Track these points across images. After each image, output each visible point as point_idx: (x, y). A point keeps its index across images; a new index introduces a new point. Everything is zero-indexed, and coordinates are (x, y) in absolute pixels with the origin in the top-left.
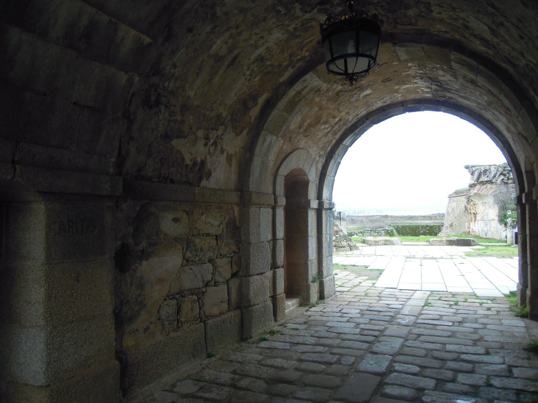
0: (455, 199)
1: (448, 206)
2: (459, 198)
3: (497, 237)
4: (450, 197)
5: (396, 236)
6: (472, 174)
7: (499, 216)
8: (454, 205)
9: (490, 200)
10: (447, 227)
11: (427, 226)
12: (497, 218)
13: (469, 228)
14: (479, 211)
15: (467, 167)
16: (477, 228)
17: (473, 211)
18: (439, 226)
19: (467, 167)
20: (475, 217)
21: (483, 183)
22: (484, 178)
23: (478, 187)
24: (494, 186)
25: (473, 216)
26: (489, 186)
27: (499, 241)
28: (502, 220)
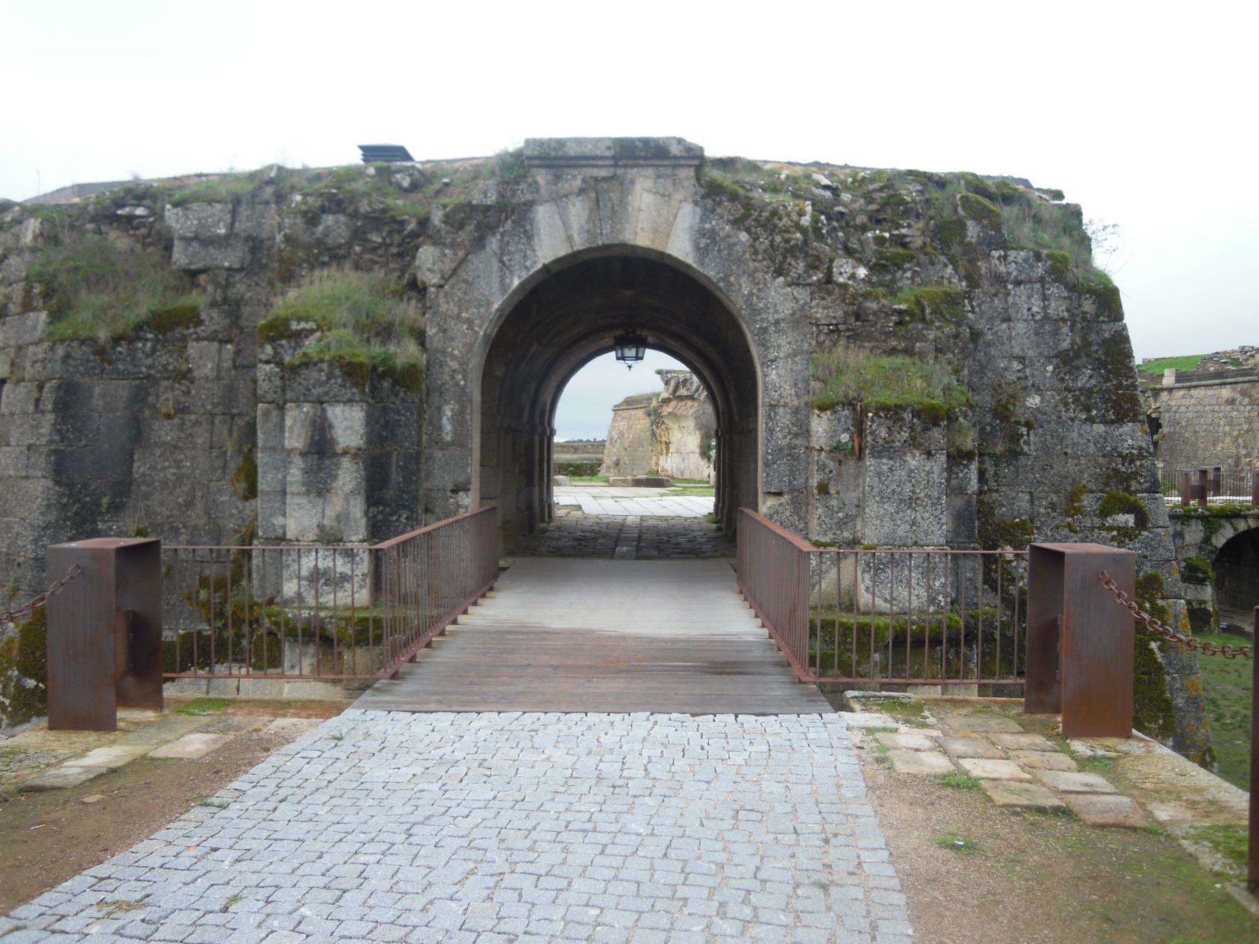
0: (626, 414)
1: (612, 428)
2: (633, 412)
3: (697, 477)
4: (616, 409)
5: (481, 505)
6: (667, 383)
7: (701, 447)
8: (622, 425)
9: (690, 423)
10: (608, 467)
11: (571, 465)
12: (698, 450)
13: (657, 464)
14: (673, 439)
15: (659, 372)
16: (669, 464)
17: (664, 439)
18: (592, 466)
19: (659, 372)
20: (668, 449)
21: (681, 398)
22: (683, 392)
23: (673, 403)
24: (696, 404)
25: (664, 446)
26: (689, 403)
27: (699, 482)
28: (704, 453)
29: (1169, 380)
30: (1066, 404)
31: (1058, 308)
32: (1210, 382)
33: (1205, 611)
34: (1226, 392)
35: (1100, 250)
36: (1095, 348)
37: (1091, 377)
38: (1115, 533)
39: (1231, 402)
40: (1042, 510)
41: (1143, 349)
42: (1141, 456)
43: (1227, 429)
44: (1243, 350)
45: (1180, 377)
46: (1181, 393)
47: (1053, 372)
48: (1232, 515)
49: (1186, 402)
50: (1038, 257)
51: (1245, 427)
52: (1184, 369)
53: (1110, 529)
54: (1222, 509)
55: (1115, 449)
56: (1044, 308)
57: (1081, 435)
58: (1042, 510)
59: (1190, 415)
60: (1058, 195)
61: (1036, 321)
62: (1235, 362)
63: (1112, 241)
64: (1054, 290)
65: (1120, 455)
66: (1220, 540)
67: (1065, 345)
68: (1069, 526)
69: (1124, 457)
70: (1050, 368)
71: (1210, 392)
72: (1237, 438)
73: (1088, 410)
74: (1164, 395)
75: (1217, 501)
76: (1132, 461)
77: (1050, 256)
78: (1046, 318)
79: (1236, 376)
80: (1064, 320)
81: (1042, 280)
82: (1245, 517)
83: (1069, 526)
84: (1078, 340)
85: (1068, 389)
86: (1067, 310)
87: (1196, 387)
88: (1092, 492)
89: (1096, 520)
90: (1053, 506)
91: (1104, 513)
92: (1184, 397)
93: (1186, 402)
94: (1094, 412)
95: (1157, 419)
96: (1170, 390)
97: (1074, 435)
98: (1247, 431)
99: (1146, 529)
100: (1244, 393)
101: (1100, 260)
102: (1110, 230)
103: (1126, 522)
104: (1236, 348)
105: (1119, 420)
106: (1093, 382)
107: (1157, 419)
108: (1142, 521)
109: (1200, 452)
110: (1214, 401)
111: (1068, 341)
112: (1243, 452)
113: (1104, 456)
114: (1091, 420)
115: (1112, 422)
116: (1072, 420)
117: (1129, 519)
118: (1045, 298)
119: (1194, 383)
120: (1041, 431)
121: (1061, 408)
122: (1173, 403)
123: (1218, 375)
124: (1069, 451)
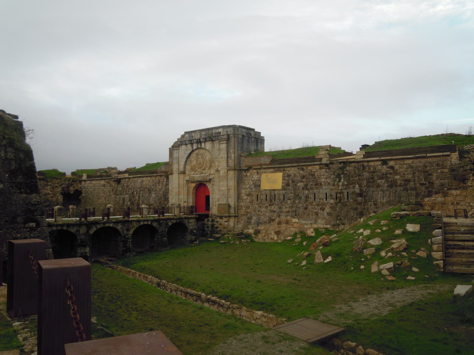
29: (85, 177)
30: (13, 188)
31: (10, 155)
32: (97, 179)
33: (87, 256)
34: (102, 182)
35: (28, 137)
36: (24, 169)
37: (22, 178)
38: (29, 229)
39: (104, 185)
40: (2, 223)
41: (38, 168)
42: (38, 204)
43: (103, 194)
44: (109, 168)
45: (88, 176)
46: (89, 182)
47: (8, 177)
48: (95, 223)
49: (91, 185)
50: (4, 138)
51: (108, 194)
52: (90, 174)
53: (27, 228)
54: (92, 221)
55: (29, 202)
56: (6, 155)
57: (17, 198)
58: (2, 223)
59: (91, 190)
60: (16, 117)
61: (2, 159)
62: (106, 172)
63: (31, 135)
64: (9, 149)
65: (31, 204)
66: (92, 232)
67: (13, 168)
68: (13, 228)
69: (32, 205)
70: (7, 175)
71: (98, 182)
72: (106, 197)
73: (20, 189)
74: (83, 183)
75: (92, 218)
76: (35, 206)
77: (8, 138)
78: (6, 159)
79: (105, 177)
80: (12, 159)
81: (5, 146)
82: (100, 224)
83: (13, 228)
84: (17, 166)
85: (13, 182)
86: (14, 156)
87: (93, 180)
88: (21, 216)
89: (22, 225)
90: (6, 221)
91: (25, 223)
92: (89, 183)
93: (91, 185)
94: (23, 190)
95: (81, 191)
96: (85, 181)
97: (15, 197)
98: (109, 195)
99: (39, 227)
100: (108, 183)
101: (28, 141)
102: (31, 131)
103: (33, 225)
104: (106, 167)
105: (31, 193)
106: (22, 180)
107: (81, 191)
108: (38, 225)
109: (94, 203)
110: (99, 185)
111: (14, 166)
112: (107, 202)
113: (26, 204)
114: (21, 193)
115: (29, 193)
116: (15, 192)
117: (34, 225)
118: (6, 152)
119: (93, 179)
120: (3, 196)
121: (11, 188)
122: (86, 185)
123: (100, 176)
124: (13, 203)
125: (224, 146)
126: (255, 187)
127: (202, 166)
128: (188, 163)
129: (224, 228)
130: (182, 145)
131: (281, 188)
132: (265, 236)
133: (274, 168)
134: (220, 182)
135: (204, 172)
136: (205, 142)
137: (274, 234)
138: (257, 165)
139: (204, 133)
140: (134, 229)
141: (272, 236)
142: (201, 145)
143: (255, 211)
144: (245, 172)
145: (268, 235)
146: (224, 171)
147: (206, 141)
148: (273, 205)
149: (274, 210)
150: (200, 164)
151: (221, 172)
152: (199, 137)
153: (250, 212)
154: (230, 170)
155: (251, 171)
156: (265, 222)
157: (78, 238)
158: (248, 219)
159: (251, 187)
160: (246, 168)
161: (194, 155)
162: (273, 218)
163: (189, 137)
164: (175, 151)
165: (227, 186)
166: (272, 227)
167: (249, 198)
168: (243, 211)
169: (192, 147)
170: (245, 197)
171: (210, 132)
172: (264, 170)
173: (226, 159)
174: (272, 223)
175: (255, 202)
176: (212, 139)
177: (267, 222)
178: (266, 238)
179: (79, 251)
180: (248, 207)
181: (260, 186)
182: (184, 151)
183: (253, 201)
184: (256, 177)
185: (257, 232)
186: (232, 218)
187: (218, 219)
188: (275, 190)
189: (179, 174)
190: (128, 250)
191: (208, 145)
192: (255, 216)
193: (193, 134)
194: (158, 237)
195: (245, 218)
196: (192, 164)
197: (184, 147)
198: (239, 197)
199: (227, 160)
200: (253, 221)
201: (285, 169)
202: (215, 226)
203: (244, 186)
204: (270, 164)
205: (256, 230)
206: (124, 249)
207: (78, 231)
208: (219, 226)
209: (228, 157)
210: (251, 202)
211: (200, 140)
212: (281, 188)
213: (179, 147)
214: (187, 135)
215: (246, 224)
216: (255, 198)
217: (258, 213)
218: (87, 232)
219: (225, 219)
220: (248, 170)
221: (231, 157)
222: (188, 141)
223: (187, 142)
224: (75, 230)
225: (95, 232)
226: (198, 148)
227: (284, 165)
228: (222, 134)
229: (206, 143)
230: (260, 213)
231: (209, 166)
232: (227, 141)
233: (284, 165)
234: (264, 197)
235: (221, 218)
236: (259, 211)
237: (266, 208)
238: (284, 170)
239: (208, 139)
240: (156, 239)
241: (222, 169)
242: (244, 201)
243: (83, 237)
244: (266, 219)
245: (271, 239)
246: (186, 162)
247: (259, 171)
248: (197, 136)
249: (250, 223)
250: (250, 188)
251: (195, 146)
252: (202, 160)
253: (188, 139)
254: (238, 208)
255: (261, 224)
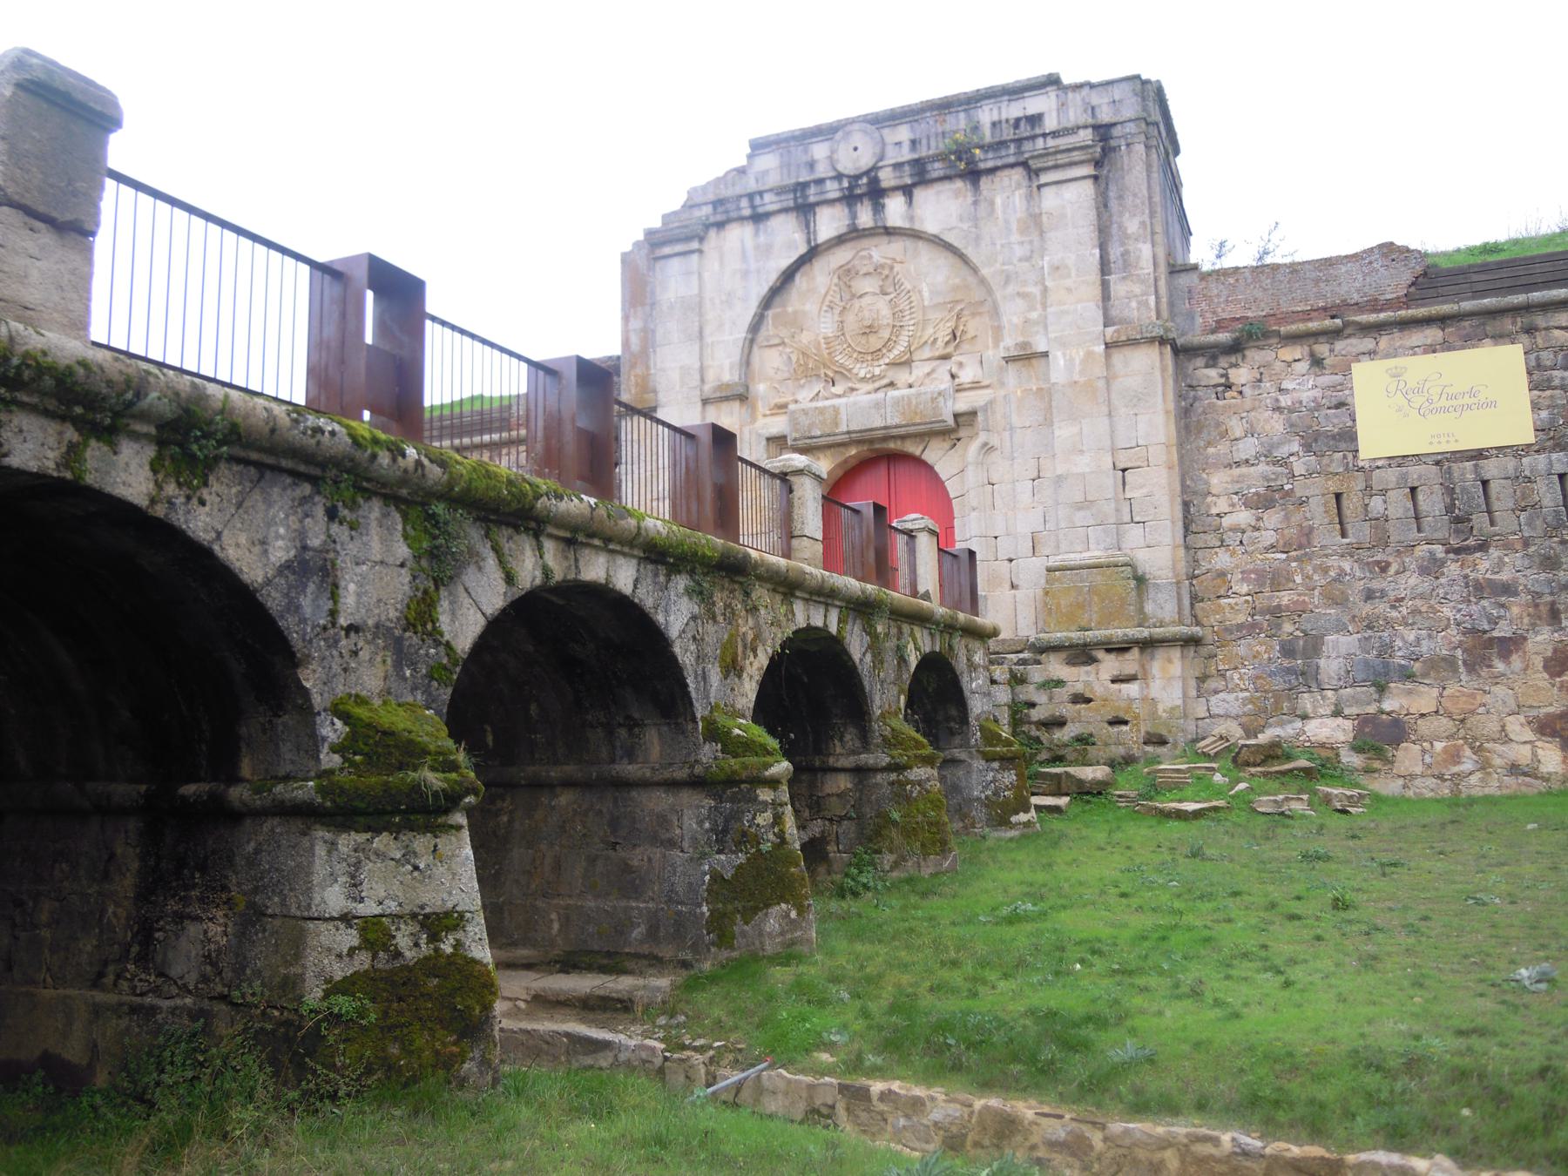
125: (1070, 199)
126: (1307, 448)
127: (888, 344)
128: (769, 330)
129: (1118, 722)
130: (720, 225)
131: (1529, 437)
132: (1454, 756)
133: (1442, 321)
134: (1048, 422)
135: (902, 377)
136: (907, 191)
137: (1529, 735)
138: (1307, 316)
139: (904, 133)
140: (763, 660)
141: (1522, 754)
142: (878, 208)
143: (1337, 599)
144: (1213, 363)
145: (1477, 750)
146: (1079, 355)
147: (919, 175)
148: (1483, 547)
149: (1505, 576)
150: (870, 330)
151: (1058, 360)
152: (865, 160)
153: (1300, 611)
154: (1132, 343)
155: (1255, 356)
156: (1441, 666)
157: (310, 679)
158: (1288, 651)
159: (1282, 452)
160: (1223, 337)
161: (821, 275)
162: (1504, 630)
163: (785, 166)
164: (675, 264)
165: (1114, 451)
166: (1500, 691)
167: (1273, 518)
168: (1235, 607)
169: (808, 228)
170: (1244, 517)
171: (958, 123)
172: (1368, 343)
173: (1094, 276)
174: (1500, 666)
175: (1326, 536)
176: (971, 161)
177: (1450, 662)
178: (1467, 766)
179: (334, 898)
180: (1277, 580)
181: (1348, 437)
182: (743, 261)
183: (1308, 533)
184: (1303, 386)
185: (1380, 737)
186: (1161, 654)
187: (1056, 667)
188: (1479, 455)
189: (705, 402)
190: (760, 883)
191: (939, 208)
192: (1341, 628)
193: (820, 151)
194: (867, 759)
195: (1262, 648)
196: (805, 338)
197: (738, 235)
198: (1192, 520)
199: (1105, 285)
200: (1330, 666)
201: (1540, 320)
202: (1035, 714)
203: (1223, 447)
204: (1408, 300)
205: (1364, 721)
206: (727, 862)
207: (315, 568)
208: (1067, 710)
209: (1105, 267)
210: (1300, 543)
211: (874, 182)
212: (1529, 437)
213: (701, 239)
214: (768, 161)
215: (1278, 684)
216: (1318, 513)
217: (1367, 609)
218: (421, 615)
219: (1110, 665)
220: (1235, 348)
221: (1127, 263)
222: (780, 191)
223: (770, 202)
224: (281, 552)
225: (496, 627)
226: (853, 234)
227: (1537, 296)
228: (1050, 124)
229: (920, 194)
230: (1381, 607)
231: (943, 335)
232: (1098, 164)
233: (1537, 296)
234: (1397, 504)
235: (1082, 654)
236: (1369, 596)
237: (1424, 571)
238: (1530, 330)
239: (937, 169)
240: (843, 782)
241: (1063, 344)
242: (1232, 539)
243: (370, 676)
244: (1444, 643)
245: (1514, 769)
246: (755, 327)
247: (1322, 349)
248: (855, 156)
249: (1309, 678)
250: (1267, 455)
251: (829, 223)
252: (885, 312)
253: (774, 180)
254: (1198, 588)
255: (1407, 676)
